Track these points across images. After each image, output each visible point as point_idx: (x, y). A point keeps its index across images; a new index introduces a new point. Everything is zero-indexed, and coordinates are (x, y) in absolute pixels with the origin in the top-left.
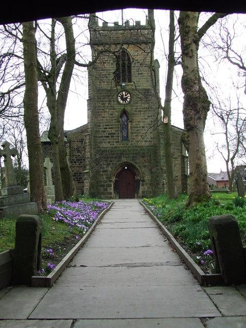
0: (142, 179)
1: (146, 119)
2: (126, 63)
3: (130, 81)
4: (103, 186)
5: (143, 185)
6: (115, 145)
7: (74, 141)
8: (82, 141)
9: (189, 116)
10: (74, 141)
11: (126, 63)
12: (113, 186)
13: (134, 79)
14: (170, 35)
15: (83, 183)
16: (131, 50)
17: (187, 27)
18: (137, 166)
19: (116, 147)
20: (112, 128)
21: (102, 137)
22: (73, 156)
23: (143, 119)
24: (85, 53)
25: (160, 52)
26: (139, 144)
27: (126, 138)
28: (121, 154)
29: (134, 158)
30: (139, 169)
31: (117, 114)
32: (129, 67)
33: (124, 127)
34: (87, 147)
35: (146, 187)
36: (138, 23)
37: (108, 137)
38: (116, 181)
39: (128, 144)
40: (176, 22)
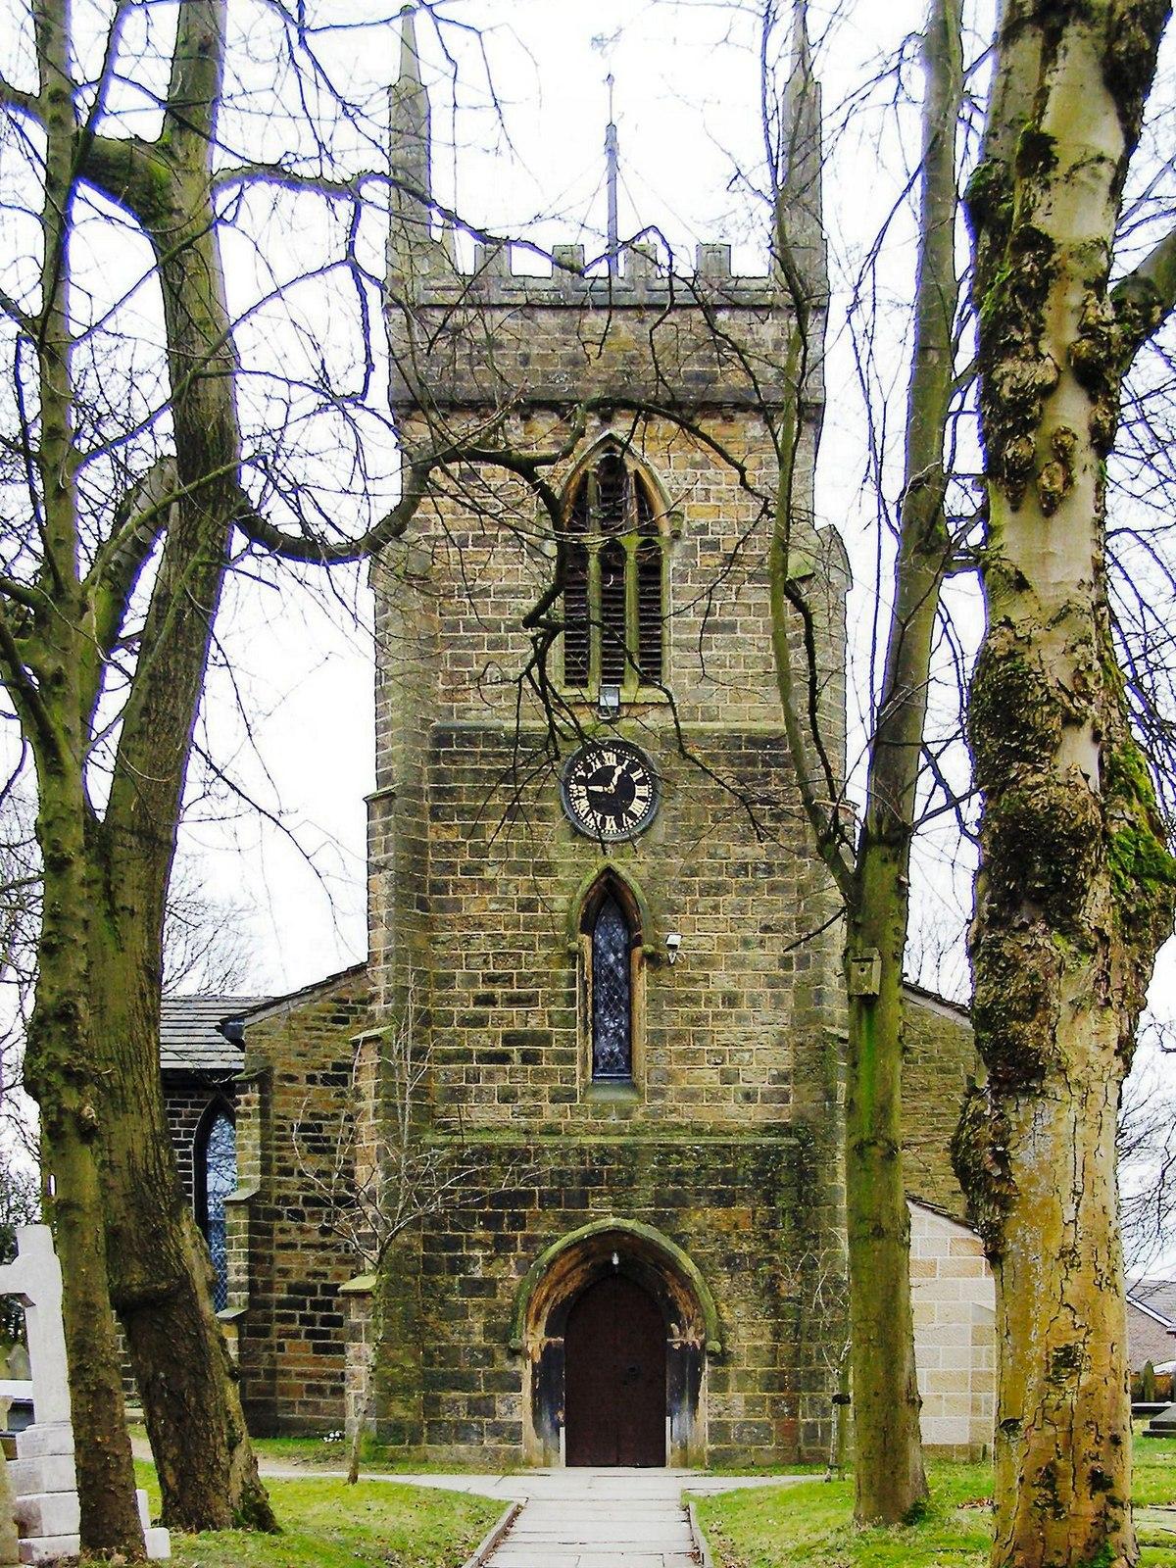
0: (714, 1345)
1: (746, 943)
2: (631, 543)
3: (651, 674)
4: (464, 1383)
5: (719, 1384)
6: (550, 1113)
7: (291, 1079)
8: (340, 1075)
9: (1017, 985)
10: (291, 1079)
11: (631, 543)
12: (526, 1392)
13: (677, 664)
14: (922, 350)
15: (341, 1349)
16: (663, 461)
17: (1038, 242)
18: (688, 1265)
19: (551, 1131)
20: (530, 1000)
21: (466, 1056)
22: (288, 1172)
23: (727, 944)
24: (342, 467)
25: (848, 488)
26: (706, 1114)
27: (617, 1066)
28: (590, 1178)
29: (668, 1209)
30: (697, 1277)
31: (560, 902)
32: (651, 572)
33: (612, 995)
34: (366, 1125)
35: (737, 1399)
36: (717, 254)
37: (503, 1058)
38: (548, 1351)
39: (626, 1114)
40: (943, 708)
